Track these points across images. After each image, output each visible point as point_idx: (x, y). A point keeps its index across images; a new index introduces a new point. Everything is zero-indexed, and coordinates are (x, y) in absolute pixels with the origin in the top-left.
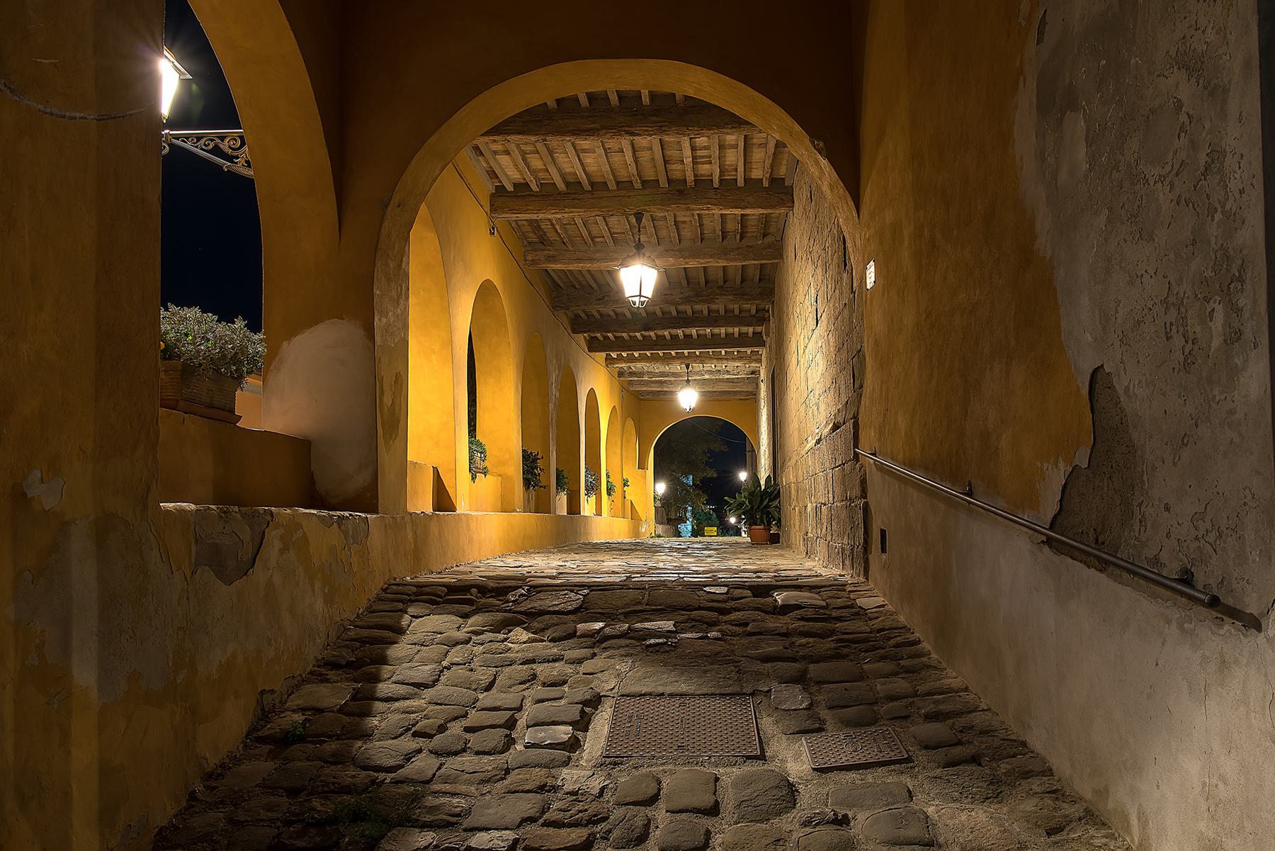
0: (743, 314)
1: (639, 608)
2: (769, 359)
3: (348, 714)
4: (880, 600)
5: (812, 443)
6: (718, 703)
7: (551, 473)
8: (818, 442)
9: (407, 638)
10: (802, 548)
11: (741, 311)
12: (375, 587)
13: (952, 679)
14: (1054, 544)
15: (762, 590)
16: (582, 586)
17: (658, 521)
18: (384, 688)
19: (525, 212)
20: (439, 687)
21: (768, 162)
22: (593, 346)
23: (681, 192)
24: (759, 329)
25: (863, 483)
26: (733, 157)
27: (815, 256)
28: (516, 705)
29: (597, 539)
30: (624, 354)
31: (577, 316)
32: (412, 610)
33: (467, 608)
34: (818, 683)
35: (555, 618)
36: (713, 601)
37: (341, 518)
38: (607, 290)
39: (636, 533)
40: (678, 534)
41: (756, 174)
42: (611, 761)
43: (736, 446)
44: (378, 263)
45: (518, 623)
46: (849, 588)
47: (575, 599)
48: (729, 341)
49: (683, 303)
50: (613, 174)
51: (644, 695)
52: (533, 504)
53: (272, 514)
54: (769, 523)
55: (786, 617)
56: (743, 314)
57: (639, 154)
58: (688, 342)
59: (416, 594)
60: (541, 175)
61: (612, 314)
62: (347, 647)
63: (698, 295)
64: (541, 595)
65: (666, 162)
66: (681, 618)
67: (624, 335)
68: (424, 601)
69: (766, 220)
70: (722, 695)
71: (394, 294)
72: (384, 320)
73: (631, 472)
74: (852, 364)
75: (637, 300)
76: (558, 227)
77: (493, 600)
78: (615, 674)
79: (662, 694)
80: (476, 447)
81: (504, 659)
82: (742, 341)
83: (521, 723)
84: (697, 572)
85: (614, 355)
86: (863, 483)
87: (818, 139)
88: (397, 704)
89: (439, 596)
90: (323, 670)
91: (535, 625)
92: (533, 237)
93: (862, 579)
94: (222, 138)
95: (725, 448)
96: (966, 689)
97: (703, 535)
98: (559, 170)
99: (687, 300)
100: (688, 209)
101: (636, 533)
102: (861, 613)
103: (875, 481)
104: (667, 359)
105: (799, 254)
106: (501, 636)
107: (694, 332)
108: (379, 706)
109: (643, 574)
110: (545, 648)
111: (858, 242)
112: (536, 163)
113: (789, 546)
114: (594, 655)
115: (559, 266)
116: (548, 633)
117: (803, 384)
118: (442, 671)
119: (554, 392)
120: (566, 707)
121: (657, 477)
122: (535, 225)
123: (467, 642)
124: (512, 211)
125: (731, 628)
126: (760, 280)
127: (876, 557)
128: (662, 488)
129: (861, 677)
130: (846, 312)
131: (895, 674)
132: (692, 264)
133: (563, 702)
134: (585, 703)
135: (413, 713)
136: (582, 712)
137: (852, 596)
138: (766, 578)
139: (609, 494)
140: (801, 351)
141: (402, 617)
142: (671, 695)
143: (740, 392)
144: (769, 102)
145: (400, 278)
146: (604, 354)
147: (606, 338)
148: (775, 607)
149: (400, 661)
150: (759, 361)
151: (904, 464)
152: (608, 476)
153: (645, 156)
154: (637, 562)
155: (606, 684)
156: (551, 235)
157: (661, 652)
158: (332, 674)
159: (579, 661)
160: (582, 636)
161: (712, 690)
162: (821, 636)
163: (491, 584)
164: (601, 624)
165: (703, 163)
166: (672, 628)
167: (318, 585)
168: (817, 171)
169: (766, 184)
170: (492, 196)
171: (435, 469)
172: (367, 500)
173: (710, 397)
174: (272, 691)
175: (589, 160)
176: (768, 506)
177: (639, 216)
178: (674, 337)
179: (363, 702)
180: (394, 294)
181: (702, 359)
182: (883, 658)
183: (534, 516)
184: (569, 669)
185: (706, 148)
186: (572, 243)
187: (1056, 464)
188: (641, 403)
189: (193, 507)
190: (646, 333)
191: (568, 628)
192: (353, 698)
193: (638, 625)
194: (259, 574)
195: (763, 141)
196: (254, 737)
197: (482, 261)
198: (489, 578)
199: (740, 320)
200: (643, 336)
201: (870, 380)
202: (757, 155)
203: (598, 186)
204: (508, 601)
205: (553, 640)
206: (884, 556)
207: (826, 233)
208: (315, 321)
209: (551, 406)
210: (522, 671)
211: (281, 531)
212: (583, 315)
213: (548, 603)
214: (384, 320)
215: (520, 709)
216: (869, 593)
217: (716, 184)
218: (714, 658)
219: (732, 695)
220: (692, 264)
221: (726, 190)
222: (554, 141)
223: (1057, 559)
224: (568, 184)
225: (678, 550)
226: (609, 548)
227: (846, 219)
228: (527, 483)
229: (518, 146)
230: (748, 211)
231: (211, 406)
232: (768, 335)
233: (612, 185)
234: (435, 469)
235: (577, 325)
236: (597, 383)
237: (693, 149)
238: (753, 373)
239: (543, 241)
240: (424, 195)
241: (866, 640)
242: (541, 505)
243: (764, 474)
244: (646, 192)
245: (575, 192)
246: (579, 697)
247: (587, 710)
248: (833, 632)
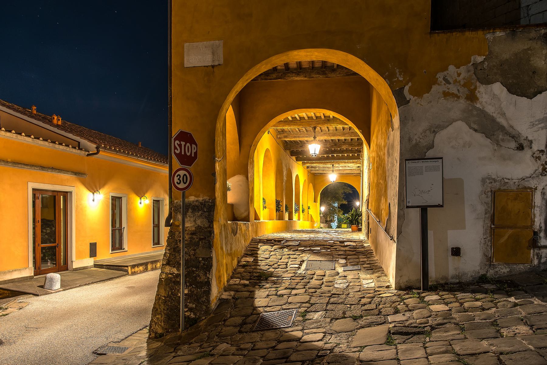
7: (285, 206)
17: (321, 222)
22: (297, 160)
23: (328, 120)
39: (312, 226)
42: (307, 269)
47: (297, 243)
54: (358, 224)
73: (311, 204)
78: (306, 257)
83: (289, 264)
97: (341, 228)
101: (313, 227)
119: (285, 178)
120: (298, 261)
121: (321, 205)
128: (323, 209)
154: (312, 235)
173: (342, 175)
176: (358, 219)
179: (256, 261)
186: (293, 132)
188: (315, 178)
196: (238, 266)
199: (351, 151)
208: (234, 175)
210: (288, 256)
218: (328, 254)
225: (326, 233)
226: (299, 232)
235: (292, 154)
236: (299, 171)
242: (281, 218)
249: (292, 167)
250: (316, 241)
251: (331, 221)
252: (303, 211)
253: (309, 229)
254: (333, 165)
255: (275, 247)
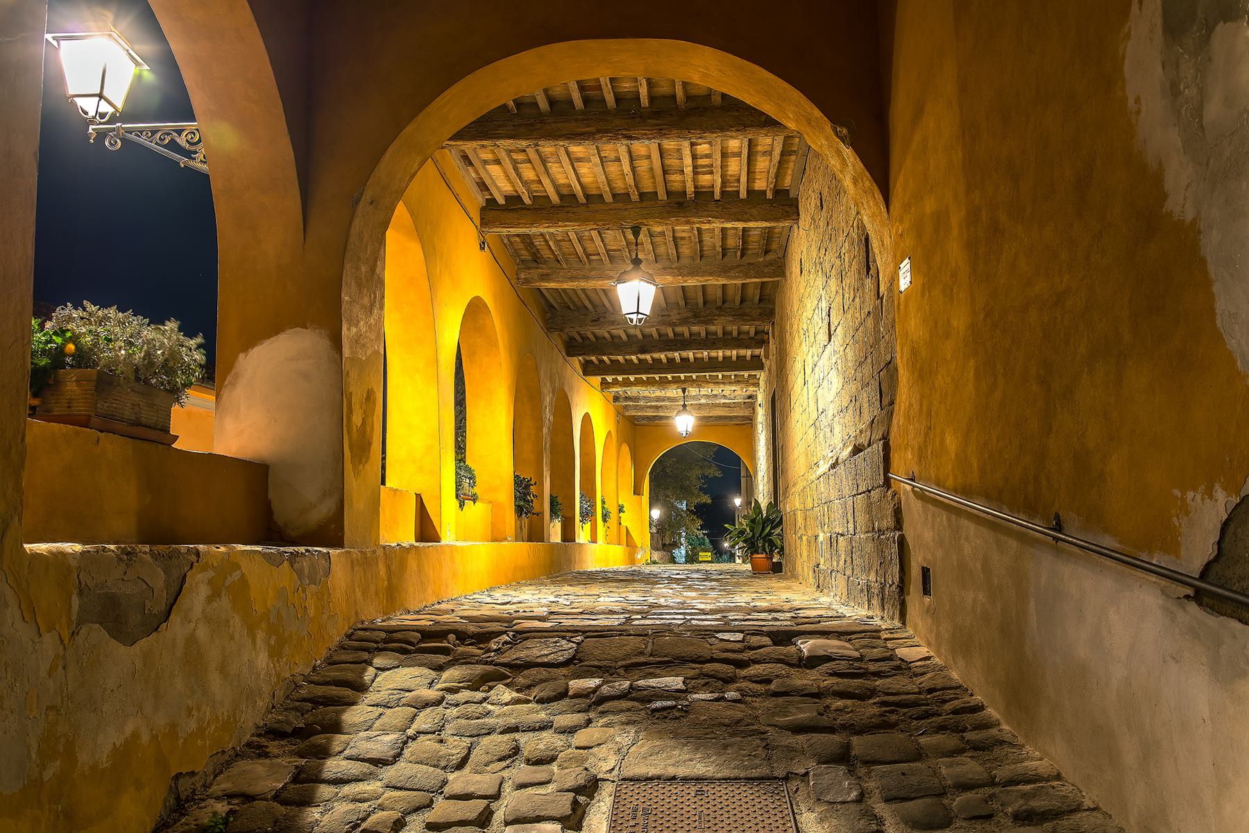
0: (742, 336)
1: (642, 659)
2: (768, 382)
3: (285, 803)
4: (923, 651)
5: (824, 467)
6: (746, 793)
7: (544, 502)
8: (833, 466)
9: (371, 697)
10: (812, 580)
11: (739, 333)
12: (336, 635)
13: (1036, 760)
14: (1206, 600)
15: (783, 637)
16: (576, 631)
17: (654, 548)
18: (334, 766)
19: (517, 226)
20: (401, 764)
21: (773, 171)
22: (588, 369)
23: (680, 205)
24: (757, 352)
25: (898, 513)
26: (735, 167)
27: (827, 266)
28: (492, 791)
29: (592, 566)
30: (620, 378)
31: (572, 339)
32: (378, 661)
33: (442, 659)
34: (867, 763)
35: (543, 673)
36: (727, 651)
37: (294, 555)
38: (604, 310)
39: (632, 560)
40: (673, 560)
41: (760, 185)
43: (727, 468)
44: (348, 266)
45: (500, 678)
46: (885, 635)
47: (566, 648)
48: (726, 365)
49: (680, 325)
50: (609, 185)
51: (651, 779)
52: (525, 531)
53: (198, 554)
55: (814, 671)
56: (742, 336)
57: (637, 163)
58: (685, 365)
59: (386, 641)
60: (534, 187)
61: (607, 335)
62: (296, 709)
63: (695, 316)
64: (528, 643)
65: (665, 172)
66: (691, 673)
67: (620, 358)
68: (392, 650)
69: (768, 235)
70: (749, 779)
71: (366, 301)
72: (354, 330)
73: (626, 498)
74: (879, 379)
75: (634, 317)
76: (551, 243)
77: (476, 649)
79: (674, 778)
80: (464, 473)
81: (481, 727)
82: (741, 364)
83: (499, 816)
84: (703, 612)
85: (609, 379)
86: (898, 513)
87: (842, 125)
88: (347, 789)
89: (411, 644)
90: (263, 741)
91: (521, 680)
92: (525, 255)
93: (897, 623)
94: (179, 132)
95: (718, 474)
96: (1058, 777)
98: (553, 181)
99: (684, 321)
100: (688, 223)
101: (632, 560)
102: (903, 667)
103: (914, 511)
104: (663, 383)
105: (806, 267)
106: (479, 695)
107: (691, 355)
108: (325, 791)
109: (644, 614)
110: (531, 711)
111: (887, 241)
112: (529, 174)
113: (794, 576)
114: (589, 722)
115: (552, 285)
116: (535, 692)
117: (812, 404)
118: (405, 743)
119: (548, 415)
122: (527, 240)
123: (438, 702)
124: (503, 224)
125: (752, 686)
126: (760, 300)
127: (915, 600)
128: (656, 513)
129: (918, 755)
130: (870, 322)
131: (959, 751)
132: (692, 282)
133: (551, 788)
134: (577, 790)
135: (365, 801)
136: (575, 803)
137: (889, 645)
138: (784, 622)
139: (605, 521)
140: (808, 371)
141: (365, 670)
142: (685, 779)
143: (736, 417)
144: (786, 85)
145: (373, 283)
146: (599, 378)
147: (602, 361)
148: (801, 659)
149: (357, 728)
150: (757, 385)
151: (955, 491)
152: (603, 502)
153: (643, 165)
154: (635, 595)
155: (604, 762)
156: (546, 253)
157: (665, 717)
158: (273, 747)
159: (571, 730)
160: (576, 696)
161: (736, 773)
162: (862, 697)
163: (472, 628)
164: (597, 681)
165: (704, 173)
166: (681, 686)
167: (260, 635)
168: (839, 161)
169: (769, 195)
170: (483, 209)
171: (419, 497)
172: (330, 533)
173: (706, 422)
174: (193, 774)
175: (584, 170)
176: (770, 534)
177: (636, 231)
178: (671, 361)
179: (303, 788)
180: (366, 301)
181: (699, 383)
182: (941, 728)
183: (525, 546)
184: (558, 741)
185: (707, 156)
186: (566, 261)
187: (1210, 493)
188: (636, 428)
189: (78, 547)
190: (642, 356)
191: (558, 685)
192: (295, 780)
193: (641, 683)
194: (176, 628)
195: (767, 148)
197: (472, 275)
198: (471, 619)
199: (738, 342)
200: (640, 360)
201: (905, 394)
202: (762, 164)
203: (593, 199)
204: (489, 651)
205: (541, 701)
206: (927, 599)
207: (841, 238)
208: (274, 330)
209: (545, 430)
210: (500, 742)
211: (211, 574)
212: (578, 338)
213: (536, 652)
214: (354, 330)
215: (497, 796)
216: (910, 642)
217: (717, 196)
218: (734, 727)
219: (761, 779)
220: (692, 282)
221: (728, 202)
222: (547, 148)
223: (1213, 621)
224: (562, 197)
227: (873, 216)
228: (520, 510)
229: (509, 152)
230: (751, 225)
231: (137, 424)
232: (767, 357)
233: (608, 198)
234: (419, 497)
235: (572, 348)
236: (591, 406)
237: (694, 157)
238: (750, 397)
239: (536, 259)
240: (399, 194)
241: (915, 704)
242: (535, 534)
243: (763, 495)
244: (644, 205)
245: (569, 205)
246: (570, 782)
247: (581, 799)
248: (873, 692)
249: (571, 388)
250: (659, 631)
251: (676, 545)
252: (605, 517)
253: (622, 568)
254: (684, 391)
255: (452, 674)
